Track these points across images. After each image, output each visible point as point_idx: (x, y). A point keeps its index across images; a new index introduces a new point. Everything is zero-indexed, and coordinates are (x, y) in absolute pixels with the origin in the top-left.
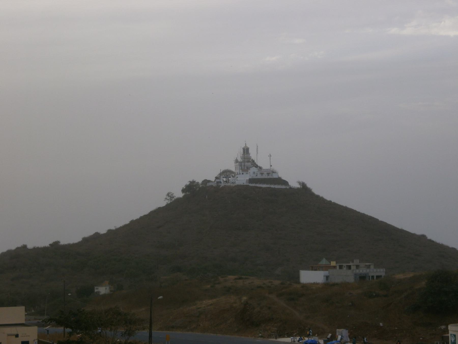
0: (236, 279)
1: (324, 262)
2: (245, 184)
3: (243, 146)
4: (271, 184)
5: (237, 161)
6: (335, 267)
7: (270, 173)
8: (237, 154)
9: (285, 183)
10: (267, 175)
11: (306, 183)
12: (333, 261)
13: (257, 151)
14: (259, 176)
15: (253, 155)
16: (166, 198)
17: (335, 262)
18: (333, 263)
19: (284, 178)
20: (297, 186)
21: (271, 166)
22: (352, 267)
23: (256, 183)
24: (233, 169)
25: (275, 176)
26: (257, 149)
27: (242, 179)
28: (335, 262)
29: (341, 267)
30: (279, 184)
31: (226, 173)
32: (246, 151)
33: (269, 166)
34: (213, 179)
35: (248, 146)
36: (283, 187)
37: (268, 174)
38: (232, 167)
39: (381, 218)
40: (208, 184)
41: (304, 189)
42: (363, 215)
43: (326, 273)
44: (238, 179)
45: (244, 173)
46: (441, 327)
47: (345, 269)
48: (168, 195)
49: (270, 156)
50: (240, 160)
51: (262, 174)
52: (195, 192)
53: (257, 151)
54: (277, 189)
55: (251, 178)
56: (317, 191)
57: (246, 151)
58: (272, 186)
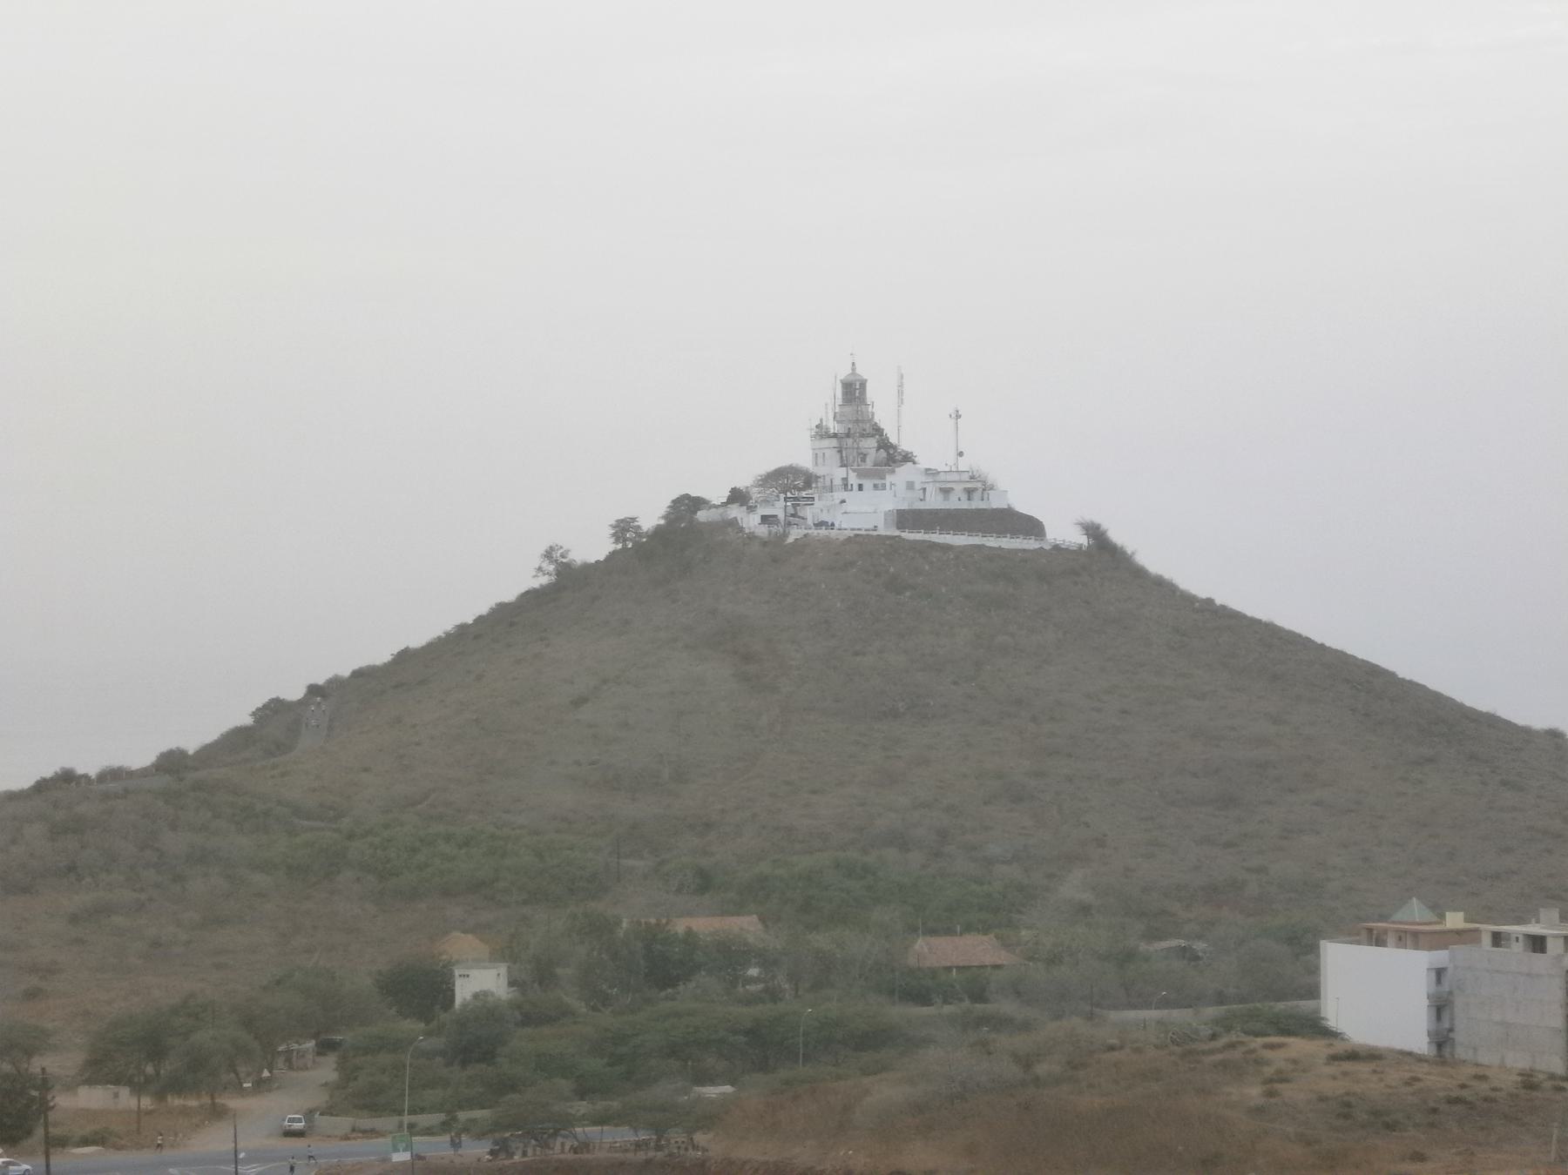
0: (197, 769)
1: (1415, 912)
2: (882, 531)
3: (844, 372)
4: (986, 531)
5: (821, 433)
6: (1459, 936)
7: (975, 490)
8: (823, 405)
9: (1032, 527)
10: (964, 497)
11: (1105, 525)
12: (1455, 910)
13: (900, 393)
14: (934, 502)
15: (882, 408)
16: (540, 569)
17: (1461, 915)
18: (1455, 920)
19: (1022, 507)
20: (1079, 539)
21: (961, 454)
22: (1550, 944)
23: (929, 528)
24: (805, 461)
25: (996, 503)
26: (901, 386)
27: (863, 510)
28: (1461, 915)
29: (1497, 939)
30: (1015, 533)
31: (790, 482)
32: (853, 391)
33: (953, 454)
34: (718, 495)
35: (862, 371)
36: (1031, 544)
37: (969, 492)
38: (801, 454)
39: (1433, 684)
40: (702, 516)
41: (1102, 550)
42: (1437, 698)
43: (1441, 957)
44: (848, 507)
45: (868, 484)
46: (460, 945)
47: (1518, 948)
48: (548, 555)
49: (958, 416)
50: (833, 427)
51: (946, 492)
52: (678, 547)
53: (900, 393)
54: (1010, 551)
55: (905, 507)
56: (1153, 557)
57: (853, 391)
58: (992, 542)
